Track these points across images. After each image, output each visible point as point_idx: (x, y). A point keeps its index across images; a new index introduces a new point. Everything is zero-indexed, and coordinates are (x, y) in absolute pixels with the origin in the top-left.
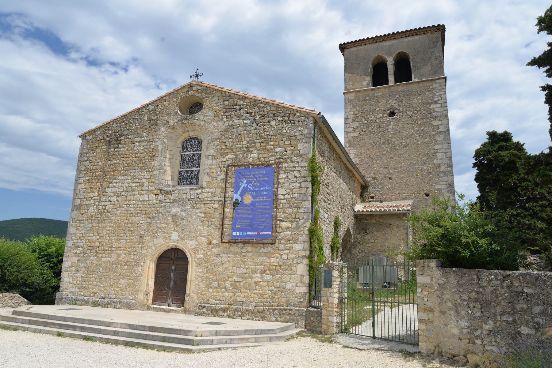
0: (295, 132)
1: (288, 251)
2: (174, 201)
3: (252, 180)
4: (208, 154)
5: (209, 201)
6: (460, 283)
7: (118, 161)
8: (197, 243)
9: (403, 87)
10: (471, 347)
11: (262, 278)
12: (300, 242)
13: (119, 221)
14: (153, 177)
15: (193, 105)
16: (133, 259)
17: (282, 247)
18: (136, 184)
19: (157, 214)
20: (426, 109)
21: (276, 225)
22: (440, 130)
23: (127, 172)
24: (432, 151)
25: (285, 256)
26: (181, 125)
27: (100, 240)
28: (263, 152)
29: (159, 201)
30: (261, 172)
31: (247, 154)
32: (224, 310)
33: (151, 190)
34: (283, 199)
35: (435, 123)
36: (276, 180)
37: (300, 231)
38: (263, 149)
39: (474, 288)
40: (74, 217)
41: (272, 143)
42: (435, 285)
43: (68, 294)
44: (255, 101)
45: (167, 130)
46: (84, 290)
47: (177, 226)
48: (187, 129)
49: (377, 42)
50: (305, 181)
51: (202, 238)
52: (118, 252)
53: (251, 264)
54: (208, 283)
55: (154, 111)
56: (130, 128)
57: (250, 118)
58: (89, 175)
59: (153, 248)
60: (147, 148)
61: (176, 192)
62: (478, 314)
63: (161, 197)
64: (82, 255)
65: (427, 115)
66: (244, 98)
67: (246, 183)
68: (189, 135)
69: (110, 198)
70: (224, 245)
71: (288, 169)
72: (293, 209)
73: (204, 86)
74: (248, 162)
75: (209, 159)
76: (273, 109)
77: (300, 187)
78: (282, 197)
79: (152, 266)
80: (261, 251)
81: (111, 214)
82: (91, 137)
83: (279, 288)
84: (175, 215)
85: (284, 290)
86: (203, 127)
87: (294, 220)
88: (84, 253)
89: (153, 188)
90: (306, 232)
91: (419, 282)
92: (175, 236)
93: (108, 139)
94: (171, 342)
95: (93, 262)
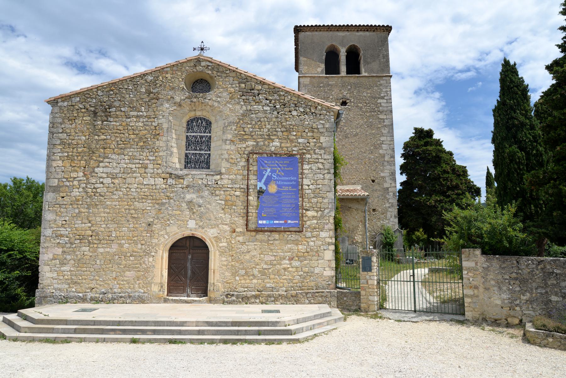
0: (317, 125)
1: (315, 239)
2: (188, 187)
3: (276, 169)
4: (225, 138)
5: (229, 188)
6: (502, 266)
7: (109, 137)
8: (219, 232)
9: (353, 79)
10: (512, 313)
11: (291, 264)
12: (326, 230)
13: (118, 207)
14: (159, 159)
15: (196, 81)
16: (141, 249)
17: (309, 234)
18: (137, 166)
19: (168, 200)
20: (374, 103)
21: (302, 214)
22: (385, 124)
23: (122, 151)
24: (379, 142)
26: (189, 103)
27: (92, 228)
28: (285, 141)
29: (169, 185)
30: (285, 162)
31: (268, 142)
32: (256, 297)
33: (157, 173)
35: (381, 116)
36: (300, 171)
37: (326, 220)
38: (285, 139)
39: (514, 270)
40: (50, 201)
42: (479, 268)
43: (54, 291)
44: (275, 88)
45: (172, 106)
46: (75, 286)
47: (194, 213)
48: (194, 108)
49: (331, 31)
50: (328, 173)
51: (224, 226)
52: (119, 242)
53: (279, 251)
54: (234, 271)
55: (154, 83)
56: (122, 99)
57: (270, 105)
58: (67, 150)
60: (147, 125)
61: (190, 176)
62: (518, 289)
63: (170, 181)
64: (68, 245)
65: (375, 109)
66: (262, 83)
67: (270, 172)
69: (101, 180)
70: (249, 233)
71: (311, 160)
73: (216, 63)
74: (270, 150)
75: (227, 144)
76: (294, 98)
77: (324, 179)
78: (307, 187)
79: (166, 255)
81: (105, 199)
82: (66, 104)
83: (308, 273)
84: (191, 202)
85: (312, 275)
86: (217, 109)
87: (320, 209)
89: (160, 171)
90: (332, 221)
91: (466, 266)
92: (192, 224)
93: (93, 109)
94: (267, 335)
95: (86, 253)
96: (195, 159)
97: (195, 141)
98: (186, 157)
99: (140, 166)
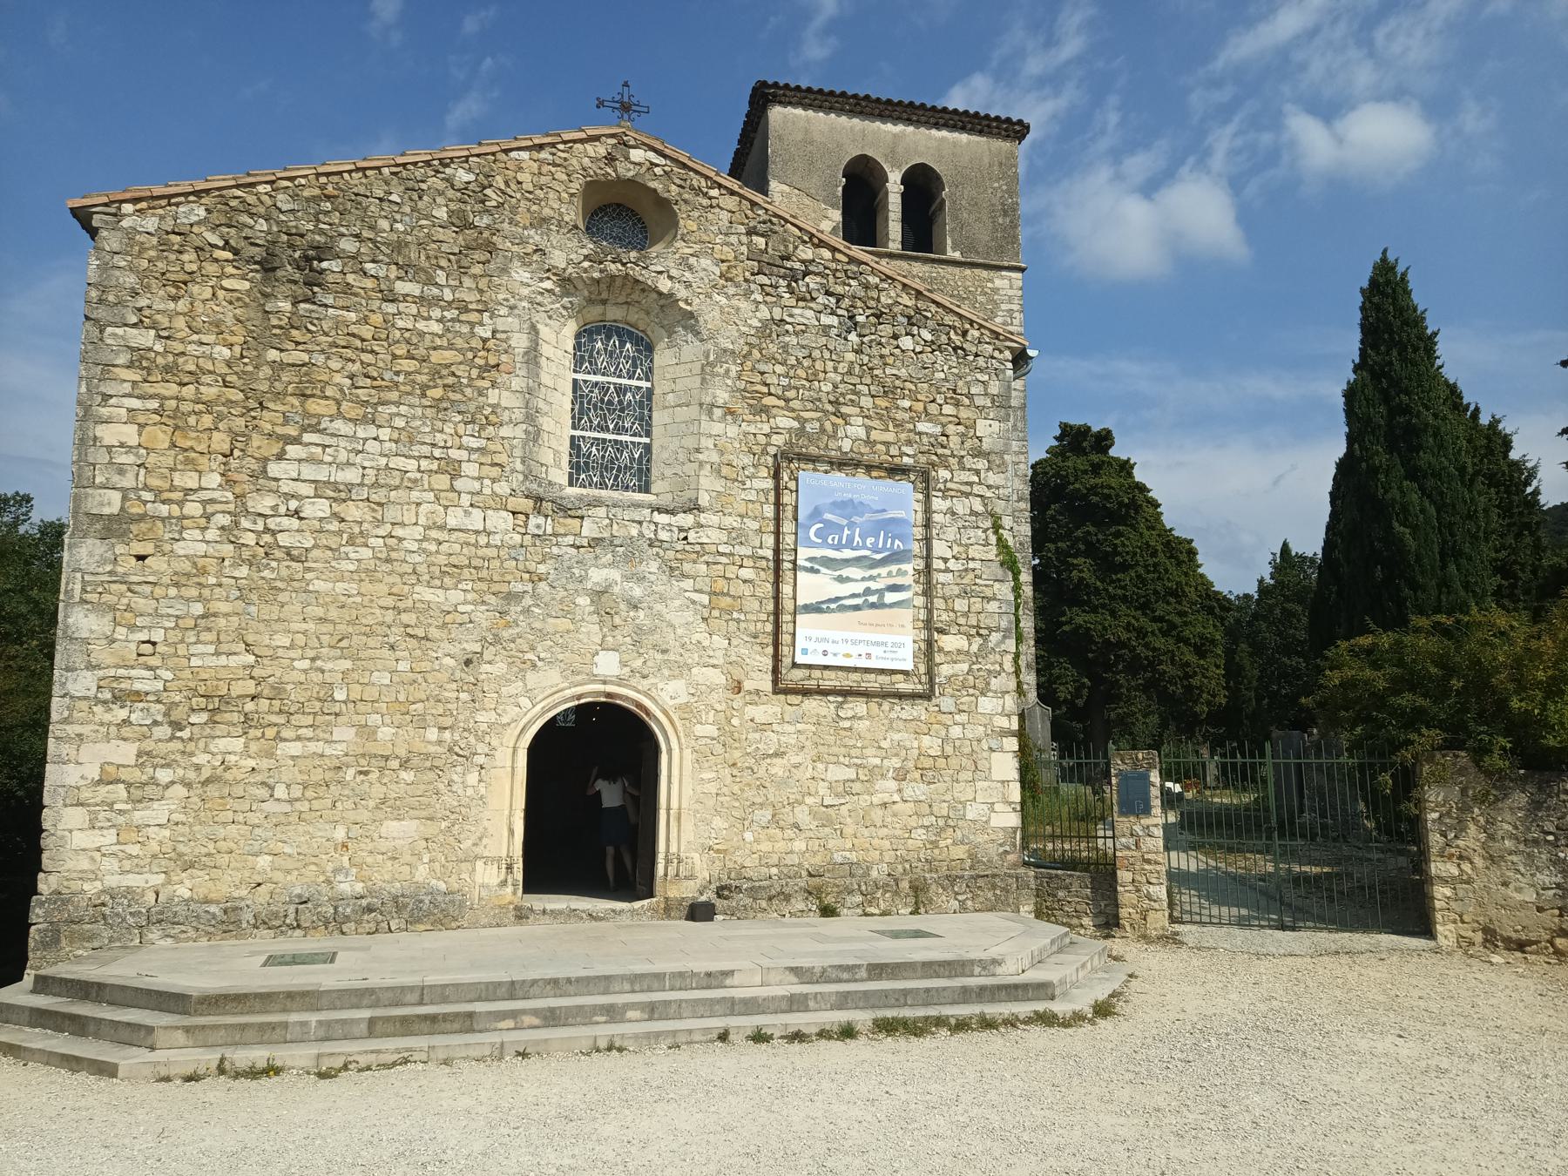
4: (708, 400)
9: (918, 271)
12: (996, 692)
16: (440, 742)
25: (956, 731)
34: (944, 571)
41: (906, 403)
48: (604, 295)
59: (524, 702)
68: (604, 314)
72: (972, 600)
80: (893, 715)
81: (309, 569)
87: (979, 632)
88: (177, 726)
96: (603, 457)
97: (602, 401)
99: (435, 466)
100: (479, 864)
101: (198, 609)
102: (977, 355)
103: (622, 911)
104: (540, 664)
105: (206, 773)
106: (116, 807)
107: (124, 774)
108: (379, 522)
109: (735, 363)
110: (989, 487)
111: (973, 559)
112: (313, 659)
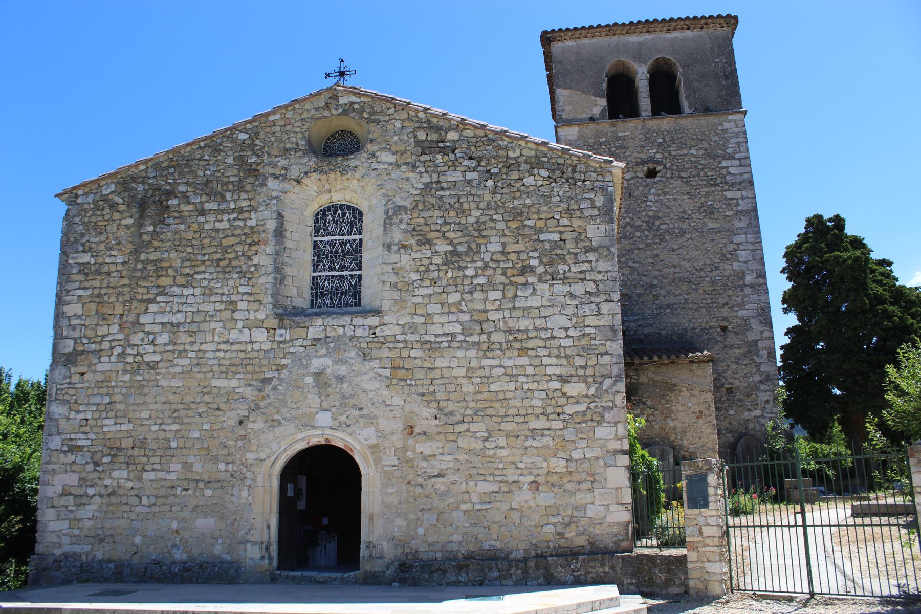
4: (388, 240)
9: (666, 123)
15: (332, 136)
18: (218, 306)
48: (327, 187)
49: (614, 35)
50: (607, 301)
65: (716, 179)
80: (528, 444)
87: (598, 379)
88: (97, 464)
96: (332, 287)
97: (331, 252)
98: (313, 284)
99: (223, 307)
100: (249, 546)
101: (107, 400)
102: (584, 181)
103: (335, 579)
104: (283, 421)
105: (110, 490)
106: (70, 508)
107: (73, 491)
108: (192, 343)
109: (406, 214)
110: (599, 272)
111: (588, 326)
112: (160, 424)
